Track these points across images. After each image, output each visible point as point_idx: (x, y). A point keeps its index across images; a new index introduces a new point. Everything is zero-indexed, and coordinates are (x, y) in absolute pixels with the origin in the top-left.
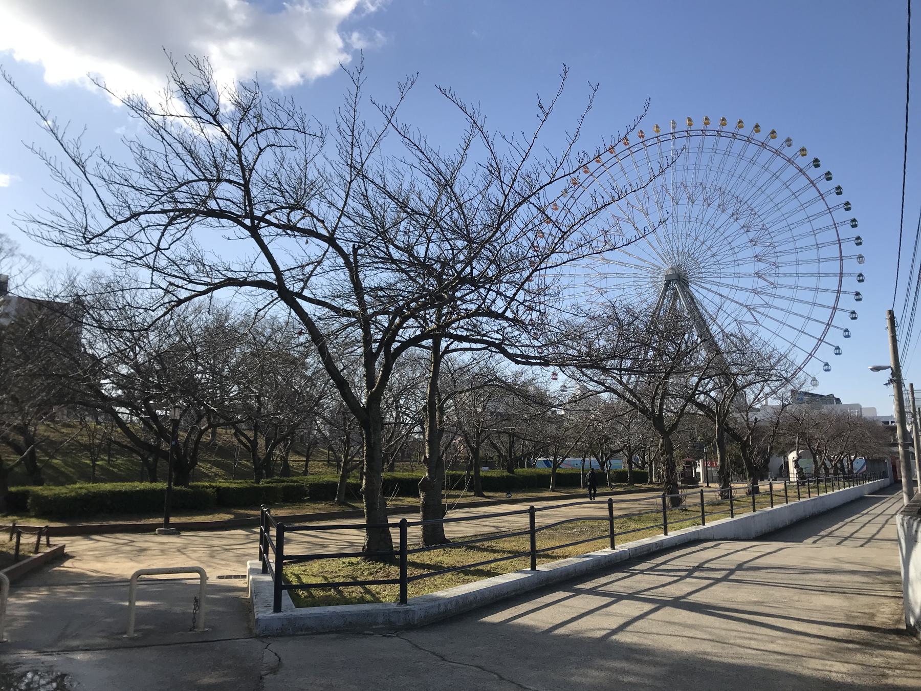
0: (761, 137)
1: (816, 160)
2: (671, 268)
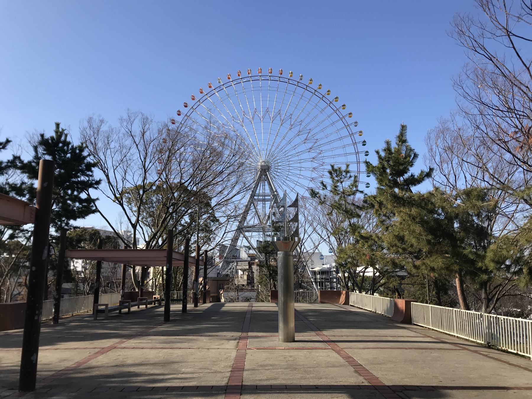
2: (263, 162)
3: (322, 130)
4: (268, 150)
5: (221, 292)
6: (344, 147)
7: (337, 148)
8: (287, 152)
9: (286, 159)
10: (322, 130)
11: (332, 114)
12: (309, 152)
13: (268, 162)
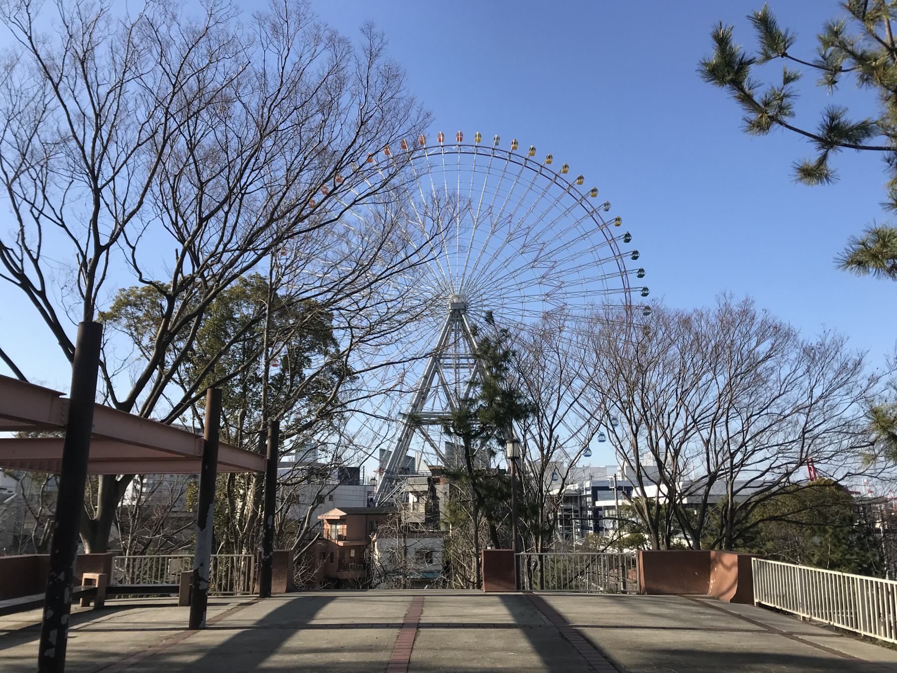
0: (607, 217)
1: (628, 235)
3: (550, 227)
4: (467, 276)
5: (374, 539)
6: (604, 278)
7: (581, 254)
8: (494, 273)
9: (494, 286)
10: (550, 227)
11: (573, 207)
12: (533, 267)
13: (463, 296)
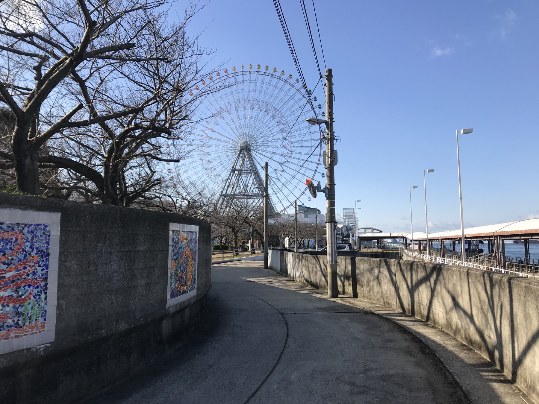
0: (285, 77)
